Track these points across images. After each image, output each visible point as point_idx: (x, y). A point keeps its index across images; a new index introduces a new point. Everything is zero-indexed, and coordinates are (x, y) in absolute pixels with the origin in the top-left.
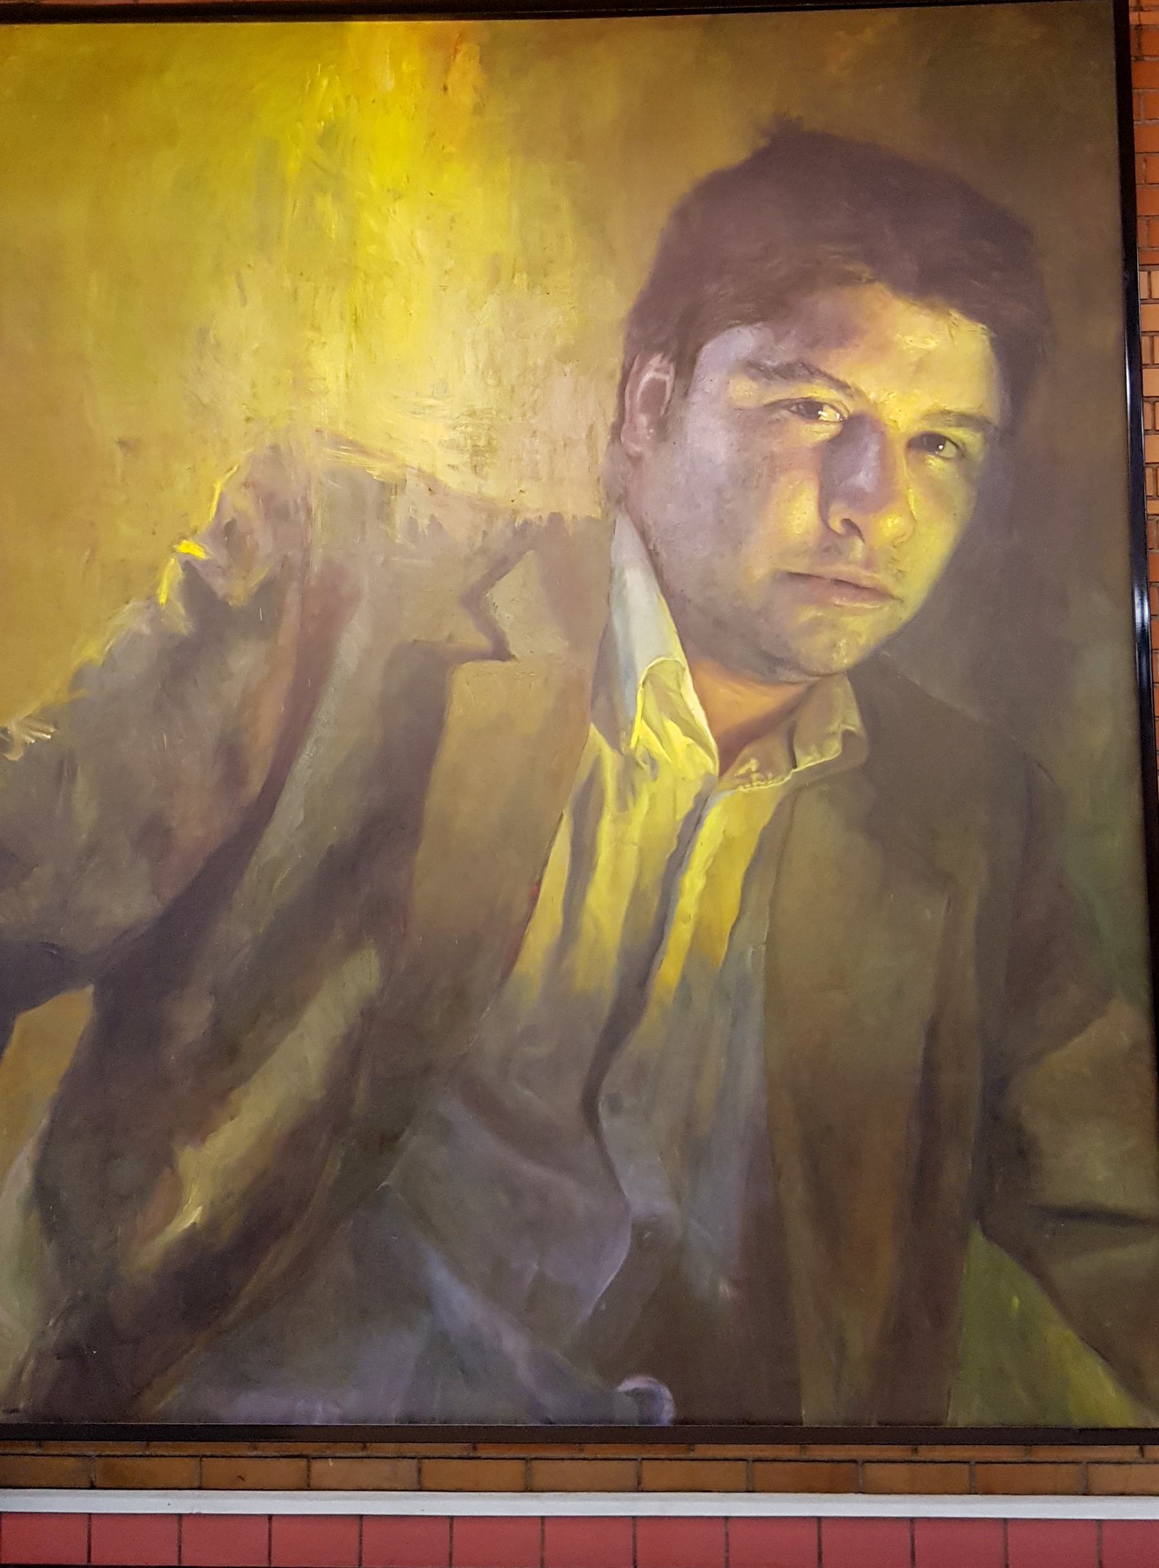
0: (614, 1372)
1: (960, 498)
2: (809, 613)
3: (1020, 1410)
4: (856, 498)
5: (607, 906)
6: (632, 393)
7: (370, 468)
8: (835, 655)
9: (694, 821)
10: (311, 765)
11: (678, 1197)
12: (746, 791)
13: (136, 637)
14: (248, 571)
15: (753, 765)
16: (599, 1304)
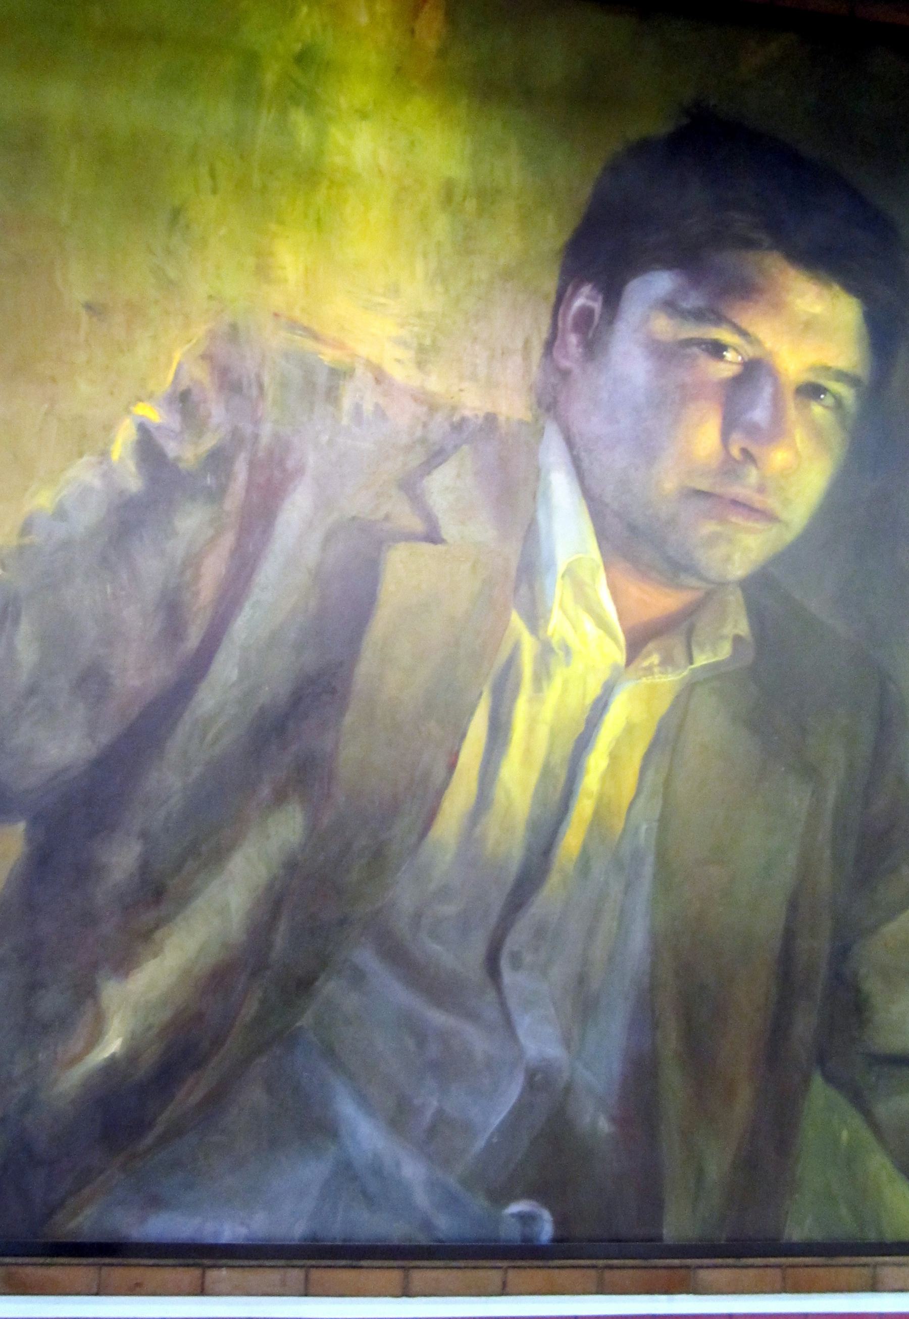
0: (501, 1196)
1: (837, 441)
2: (709, 528)
3: (845, 1226)
4: (753, 431)
5: (518, 780)
6: (565, 315)
7: (322, 354)
8: (729, 567)
9: (600, 706)
10: (244, 627)
11: (567, 1042)
12: (649, 682)
13: (86, 491)
14: (200, 437)
15: (655, 659)
16: (491, 1137)
